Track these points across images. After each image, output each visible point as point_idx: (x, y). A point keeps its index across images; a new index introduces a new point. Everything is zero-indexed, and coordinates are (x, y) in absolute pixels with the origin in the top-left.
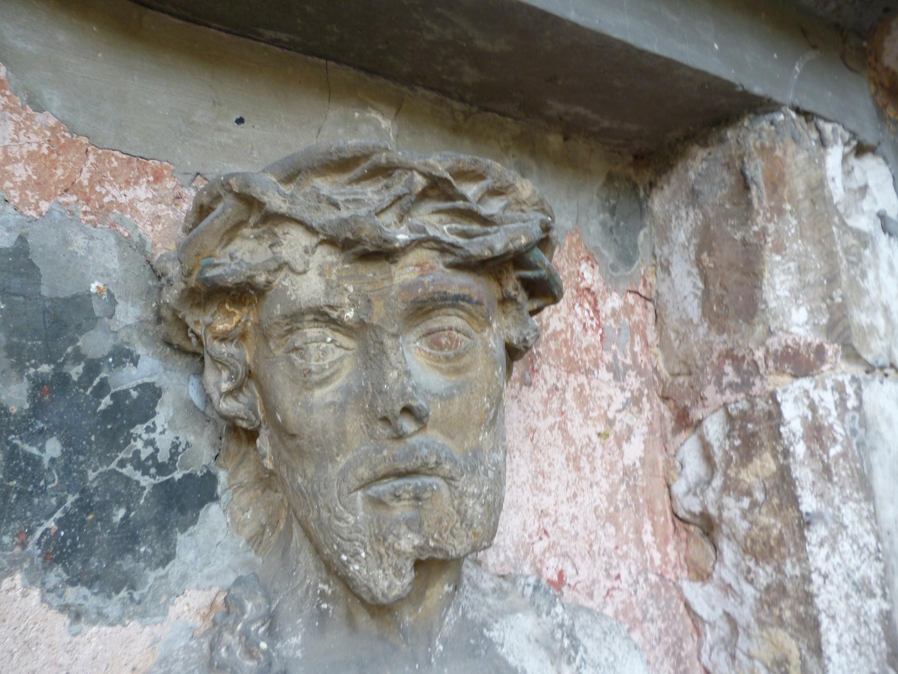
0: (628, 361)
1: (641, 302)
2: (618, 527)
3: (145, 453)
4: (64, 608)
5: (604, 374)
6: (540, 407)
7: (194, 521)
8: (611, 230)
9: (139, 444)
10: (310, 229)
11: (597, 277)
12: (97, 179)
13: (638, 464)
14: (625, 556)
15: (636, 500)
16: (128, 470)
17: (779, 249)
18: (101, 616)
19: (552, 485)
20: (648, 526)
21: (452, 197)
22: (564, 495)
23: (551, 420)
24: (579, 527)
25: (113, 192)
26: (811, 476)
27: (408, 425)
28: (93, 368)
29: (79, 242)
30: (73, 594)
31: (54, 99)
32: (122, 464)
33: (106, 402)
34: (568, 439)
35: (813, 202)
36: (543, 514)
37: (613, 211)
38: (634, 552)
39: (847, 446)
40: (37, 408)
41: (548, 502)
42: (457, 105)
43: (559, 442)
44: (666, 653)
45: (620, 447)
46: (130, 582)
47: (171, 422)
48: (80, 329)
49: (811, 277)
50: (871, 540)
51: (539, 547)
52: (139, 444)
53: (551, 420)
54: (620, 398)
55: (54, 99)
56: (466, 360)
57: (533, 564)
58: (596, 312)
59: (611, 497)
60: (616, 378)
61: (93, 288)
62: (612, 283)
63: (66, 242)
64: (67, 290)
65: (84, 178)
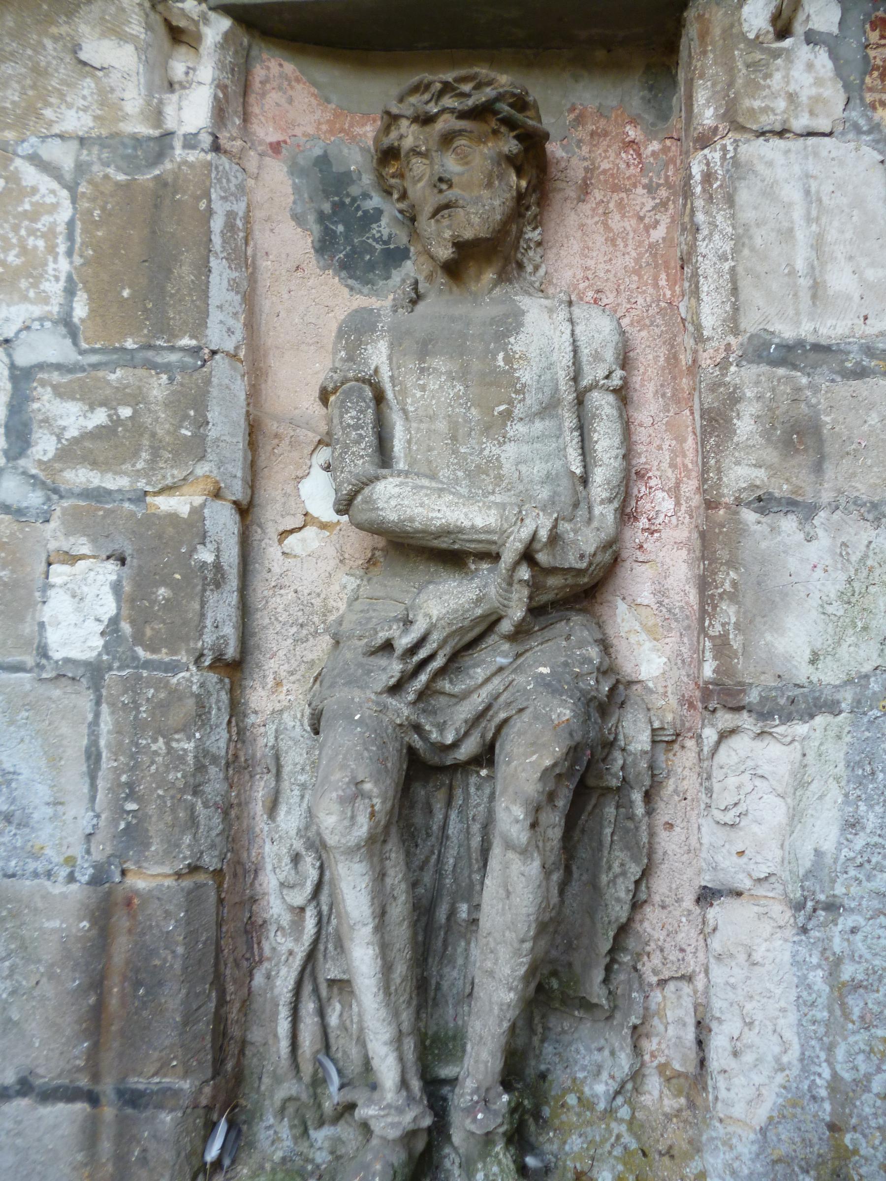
0: (662, 181)
1: (675, 142)
2: (640, 277)
3: (377, 235)
4: (347, 286)
5: (640, 190)
6: (589, 213)
7: (400, 266)
8: (649, 101)
9: (374, 232)
10: (408, 118)
11: (639, 132)
12: (351, 125)
13: (661, 241)
14: (644, 292)
15: (656, 262)
16: (370, 241)
17: (701, 76)
18: (361, 292)
19: (595, 254)
20: (663, 276)
21: (454, 89)
22: (601, 259)
23: (596, 219)
24: (611, 276)
25: (357, 130)
26: (703, 203)
27: (444, 187)
28: (354, 200)
29: (346, 151)
30: (350, 282)
31: (334, 98)
32: (368, 238)
33: (360, 213)
34: (607, 228)
35: (724, 40)
36: (587, 268)
37: (651, 88)
38: (651, 290)
39: (723, 180)
40: (334, 213)
41: (591, 263)
42: (528, 52)
43: (601, 230)
44: (664, 343)
45: (648, 232)
46: (372, 283)
47: (388, 224)
48: (348, 185)
49: (718, 88)
50: (730, 230)
51: (582, 286)
52: (374, 232)
53: (596, 219)
54: (650, 204)
55: (334, 98)
56: (469, 158)
57: (578, 294)
58: (639, 155)
59: (637, 260)
60: (649, 192)
61: (352, 168)
62: (651, 135)
63: (341, 151)
64: (342, 169)
65: (346, 126)
